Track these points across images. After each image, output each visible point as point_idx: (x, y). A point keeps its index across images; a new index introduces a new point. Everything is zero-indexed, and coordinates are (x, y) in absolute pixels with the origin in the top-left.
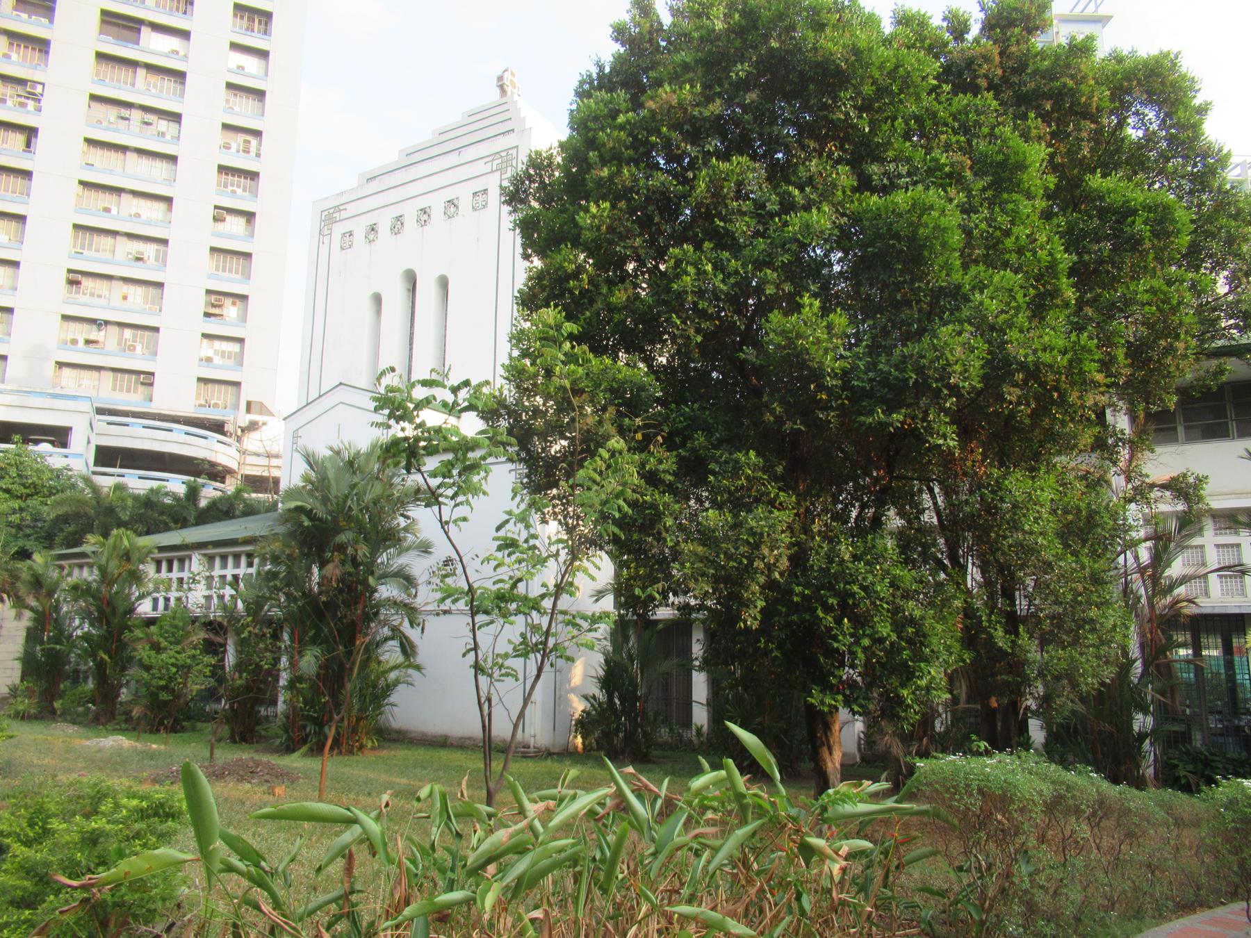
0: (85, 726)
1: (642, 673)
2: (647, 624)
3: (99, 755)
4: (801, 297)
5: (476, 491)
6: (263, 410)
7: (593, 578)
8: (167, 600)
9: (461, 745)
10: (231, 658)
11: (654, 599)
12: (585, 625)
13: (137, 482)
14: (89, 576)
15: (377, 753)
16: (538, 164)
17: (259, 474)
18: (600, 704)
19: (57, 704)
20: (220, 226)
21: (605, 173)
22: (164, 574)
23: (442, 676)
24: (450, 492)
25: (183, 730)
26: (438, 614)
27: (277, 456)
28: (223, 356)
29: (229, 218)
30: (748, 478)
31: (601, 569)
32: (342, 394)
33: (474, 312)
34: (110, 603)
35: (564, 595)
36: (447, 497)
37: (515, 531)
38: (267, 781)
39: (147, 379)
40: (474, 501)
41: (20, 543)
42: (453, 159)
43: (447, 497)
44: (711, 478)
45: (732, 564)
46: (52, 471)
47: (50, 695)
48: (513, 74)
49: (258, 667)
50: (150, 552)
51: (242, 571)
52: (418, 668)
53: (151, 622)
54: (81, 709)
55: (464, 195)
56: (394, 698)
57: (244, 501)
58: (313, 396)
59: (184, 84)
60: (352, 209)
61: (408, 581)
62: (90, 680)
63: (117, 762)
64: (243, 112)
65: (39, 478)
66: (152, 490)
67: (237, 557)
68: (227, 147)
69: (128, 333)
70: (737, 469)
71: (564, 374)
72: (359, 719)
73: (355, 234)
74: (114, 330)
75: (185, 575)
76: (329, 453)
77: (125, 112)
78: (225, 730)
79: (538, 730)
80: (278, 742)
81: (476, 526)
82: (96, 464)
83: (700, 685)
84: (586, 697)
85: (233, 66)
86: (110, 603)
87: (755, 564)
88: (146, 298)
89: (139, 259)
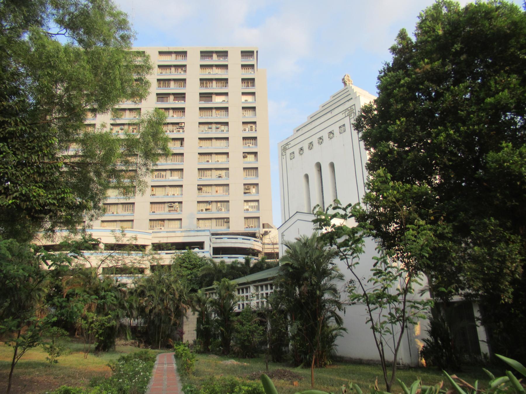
0: (220, 356)
1: (450, 329)
2: (449, 305)
3: (226, 368)
4: (501, 144)
5: (360, 251)
6: (269, 226)
7: (421, 284)
8: (243, 305)
9: (369, 363)
10: (269, 327)
11: (452, 292)
12: (421, 307)
13: (228, 260)
14: (215, 297)
15: (332, 367)
16: (367, 110)
17: (270, 252)
18: (431, 343)
19: (210, 347)
20: (246, 159)
21: (399, 107)
22: (241, 294)
23: (357, 333)
24: (350, 253)
25: (255, 357)
26: (350, 305)
27: (276, 244)
28: (252, 208)
29: (248, 156)
30: (492, 230)
31: (422, 280)
32: (298, 216)
33: (350, 175)
34: (224, 307)
35: (408, 293)
36: (349, 255)
37: (381, 266)
38: (290, 379)
39: (227, 220)
40: (360, 255)
41: (192, 286)
42: (329, 115)
43: (349, 255)
44: (473, 233)
45: (491, 272)
46: (199, 258)
47: (206, 344)
48: (348, 76)
49: (281, 331)
50: (236, 286)
51: (269, 291)
52: (344, 329)
53: (238, 314)
54: (218, 349)
55: (336, 129)
56: (336, 342)
57: (266, 263)
58: (287, 218)
59: (228, 111)
60: (293, 143)
61: (334, 291)
62: (220, 338)
63: (233, 370)
64: (249, 116)
65: (196, 261)
66: (233, 262)
67: (266, 286)
68: (245, 130)
69: (219, 204)
70: (485, 227)
71: (392, 194)
72: (322, 352)
73: (295, 153)
74: (214, 204)
75: (248, 294)
76: (296, 241)
77: (210, 126)
78: (270, 357)
79: (403, 357)
80: (291, 362)
81: (362, 266)
82: (213, 254)
83: (481, 333)
84: (424, 340)
85: (243, 100)
86: (224, 307)
87: (505, 271)
88: (224, 190)
89: (220, 177)
